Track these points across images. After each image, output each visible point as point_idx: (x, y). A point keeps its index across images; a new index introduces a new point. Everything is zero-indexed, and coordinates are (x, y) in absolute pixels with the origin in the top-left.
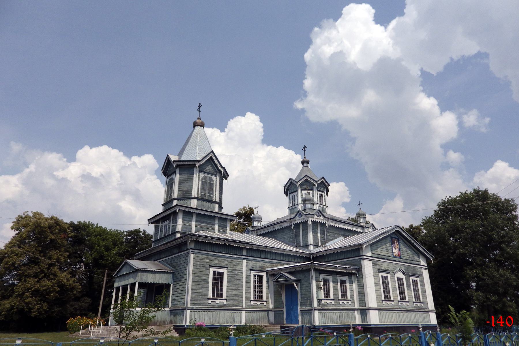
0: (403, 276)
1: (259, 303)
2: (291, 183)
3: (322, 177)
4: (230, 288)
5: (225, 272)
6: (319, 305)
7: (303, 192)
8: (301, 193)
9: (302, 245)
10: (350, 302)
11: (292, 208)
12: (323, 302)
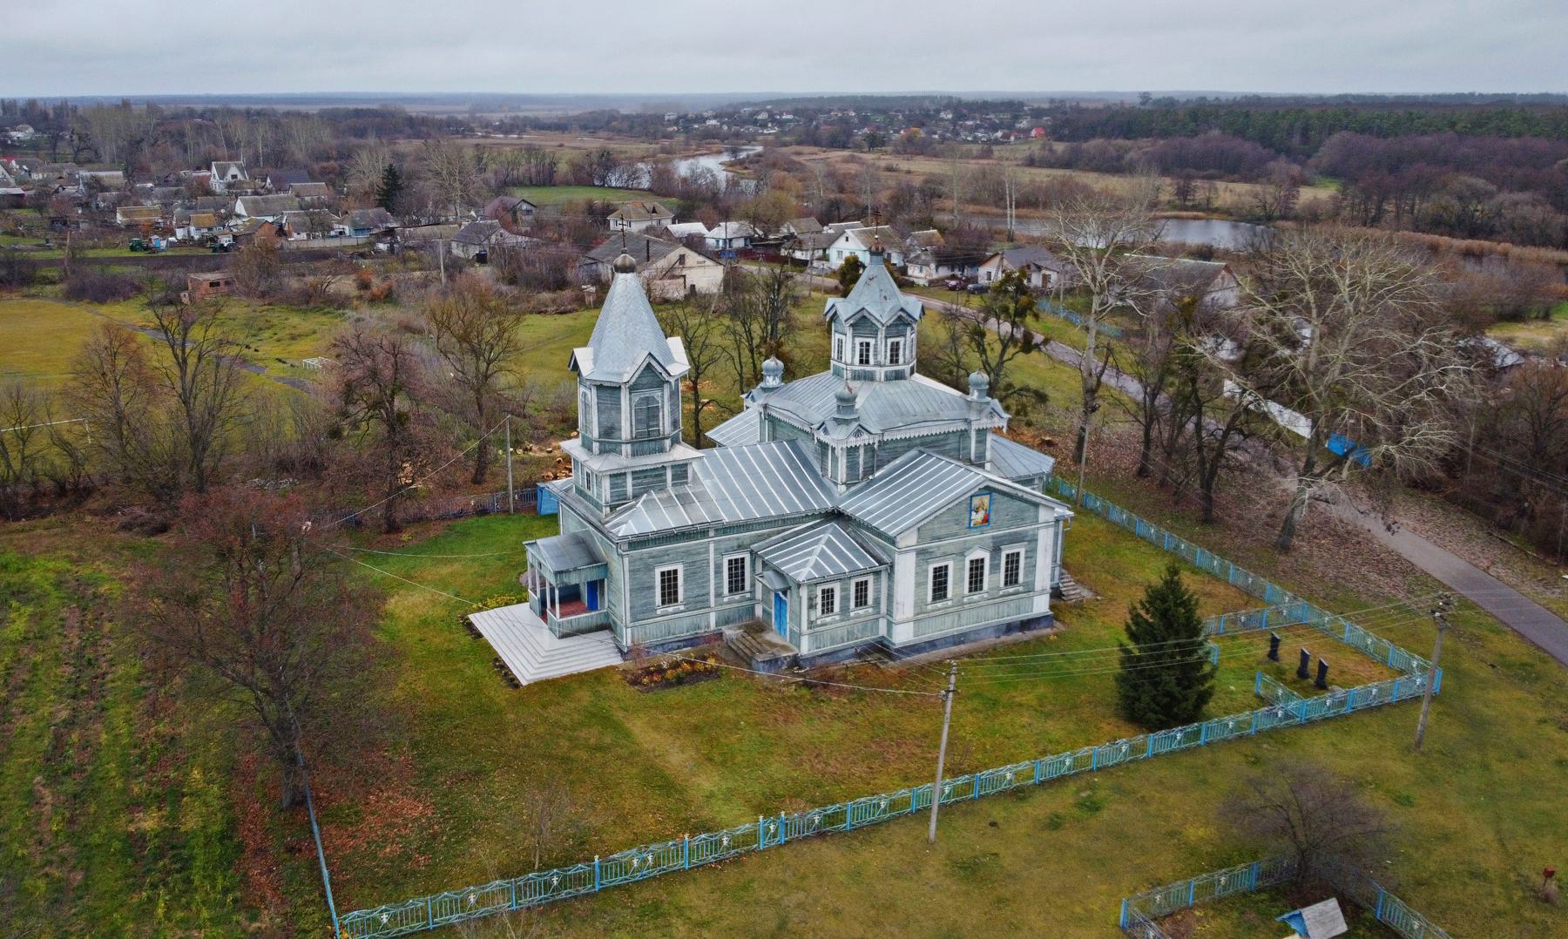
0: (986, 555)
5: (680, 568)
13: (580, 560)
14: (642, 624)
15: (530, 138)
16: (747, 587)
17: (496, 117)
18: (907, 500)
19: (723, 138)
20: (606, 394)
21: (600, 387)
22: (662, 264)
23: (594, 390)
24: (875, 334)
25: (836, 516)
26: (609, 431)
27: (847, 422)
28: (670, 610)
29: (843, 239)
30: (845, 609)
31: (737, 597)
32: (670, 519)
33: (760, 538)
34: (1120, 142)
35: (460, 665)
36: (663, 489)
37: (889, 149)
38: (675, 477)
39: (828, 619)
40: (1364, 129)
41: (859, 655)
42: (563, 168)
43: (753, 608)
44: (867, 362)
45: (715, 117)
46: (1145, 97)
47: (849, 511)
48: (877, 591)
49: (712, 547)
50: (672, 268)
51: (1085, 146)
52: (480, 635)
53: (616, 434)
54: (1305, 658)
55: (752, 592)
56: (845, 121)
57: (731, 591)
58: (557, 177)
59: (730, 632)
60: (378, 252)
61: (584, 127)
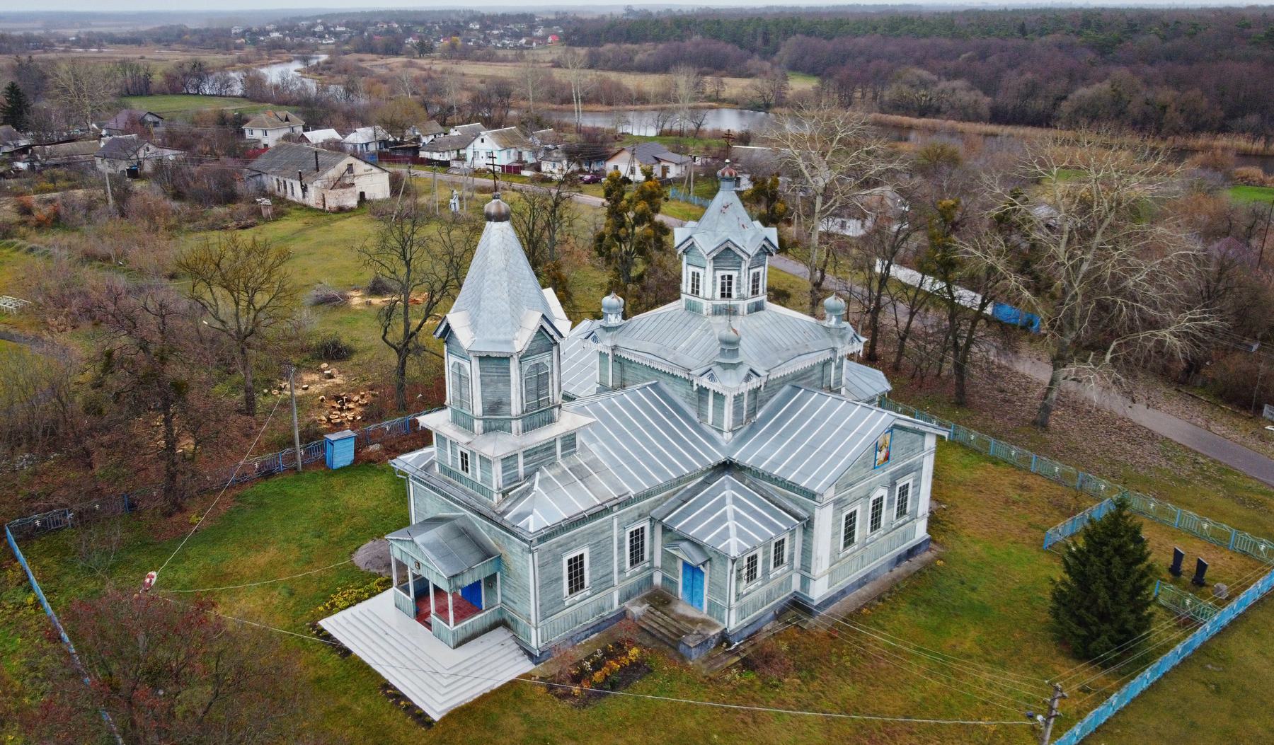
13: (467, 555)
14: (553, 620)
15: (132, 53)
16: (647, 557)
17: (71, 33)
18: (812, 447)
19: (290, 49)
20: (491, 366)
21: (484, 359)
22: (333, 173)
23: (476, 363)
24: (738, 266)
25: (727, 467)
26: (495, 407)
27: (734, 366)
28: (577, 598)
29: (479, 140)
30: (766, 573)
31: (638, 569)
32: (577, 501)
33: (658, 503)
34: (629, 46)
35: (344, 700)
36: (552, 464)
37: (437, 54)
38: (564, 448)
39: (752, 587)
40: (809, 32)
41: (777, 617)
42: (157, 79)
43: (651, 576)
44: (730, 296)
45: (277, 30)
46: (629, 10)
47: (748, 462)
48: (792, 547)
49: (615, 522)
50: (342, 177)
51: (601, 49)
52: (347, 652)
53: (505, 409)
54: (1178, 556)
55: (651, 561)
56: (390, 31)
57: (632, 564)
58: (154, 87)
59: (637, 610)
60: (18, 171)
61: (158, 41)
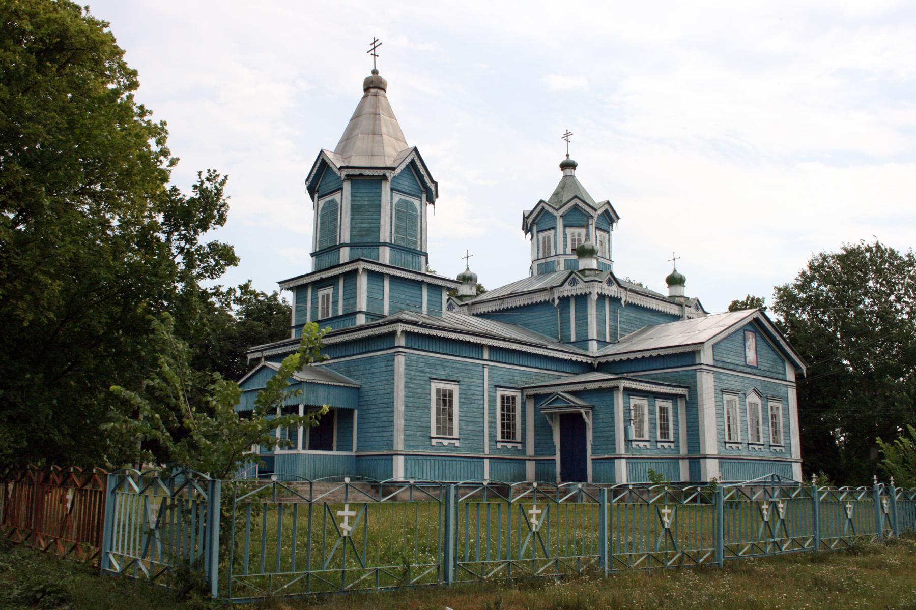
1: (509, 446)
2: (543, 209)
3: (605, 200)
4: (464, 418)
6: (627, 450)
7: (568, 230)
8: (564, 232)
9: (573, 339)
10: (672, 445)
11: (543, 267)
12: (634, 444)
